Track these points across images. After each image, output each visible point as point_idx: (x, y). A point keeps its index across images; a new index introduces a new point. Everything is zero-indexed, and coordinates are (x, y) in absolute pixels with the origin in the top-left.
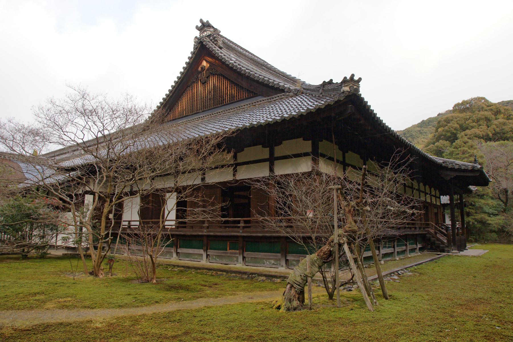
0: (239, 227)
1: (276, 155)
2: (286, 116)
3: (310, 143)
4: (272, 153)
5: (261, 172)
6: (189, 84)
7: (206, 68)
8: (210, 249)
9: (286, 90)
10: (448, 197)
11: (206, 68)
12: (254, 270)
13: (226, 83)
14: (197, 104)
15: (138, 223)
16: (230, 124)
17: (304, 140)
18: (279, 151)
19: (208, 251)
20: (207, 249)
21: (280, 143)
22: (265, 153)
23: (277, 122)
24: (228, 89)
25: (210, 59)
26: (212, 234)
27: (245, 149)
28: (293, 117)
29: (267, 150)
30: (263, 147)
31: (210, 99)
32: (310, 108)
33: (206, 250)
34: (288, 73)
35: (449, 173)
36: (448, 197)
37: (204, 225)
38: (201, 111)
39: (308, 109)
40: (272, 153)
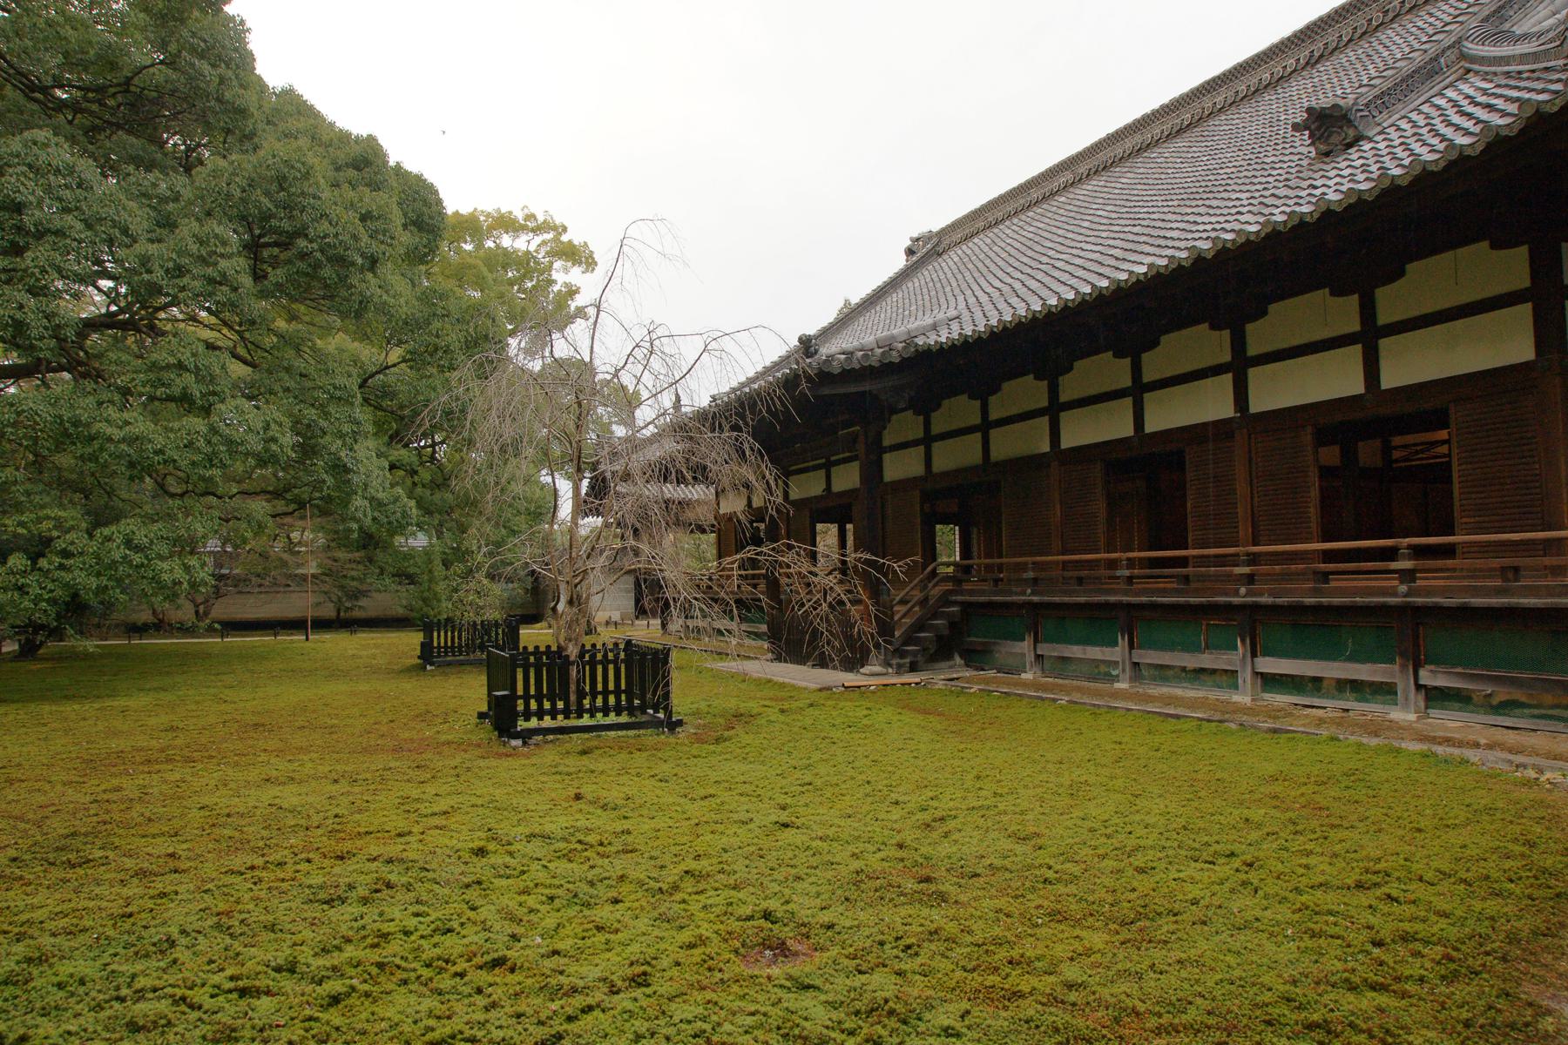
1: (1383, 319)
2: (1397, 172)
3: (1519, 256)
4: (1239, 344)
5: (1211, 404)
10: (1336, 449)
12: (1193, 648)
16: (1234, 211)
17: (1493, 247)
18: (1260, 336)
21: (1155, 343)
22: (1344, 314)
23: (1180, 267)
26: (1265, 599)
27: (1409, 267)
28: (1248, 242)
30: (1213, 327)
32: (1462, 140)
36: (1336, 449)
39: (1451, 145)
40: (1239, 344)
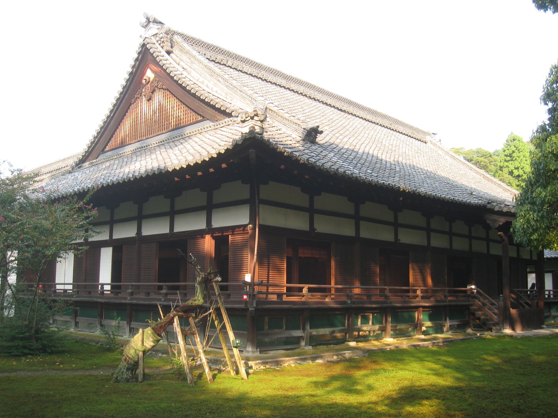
0: (161, 294)
6: (133, 100)
7: (151, 80)
8: (135, 321)
9: (233, 114)
11: (151, 80)
13: (173, 102)
14: (141, 129)
15: (71, 287)
19: (132, 323)
20: (131, 321)
24: (176, 110)
25: (155, 68)
26: (135, 302)
29: (168, 201)
31: (155, 122)
33: (129, 323)
34: (91, 138)
35: (495, 217)
37: (162, 291)
38: (145, 138)
